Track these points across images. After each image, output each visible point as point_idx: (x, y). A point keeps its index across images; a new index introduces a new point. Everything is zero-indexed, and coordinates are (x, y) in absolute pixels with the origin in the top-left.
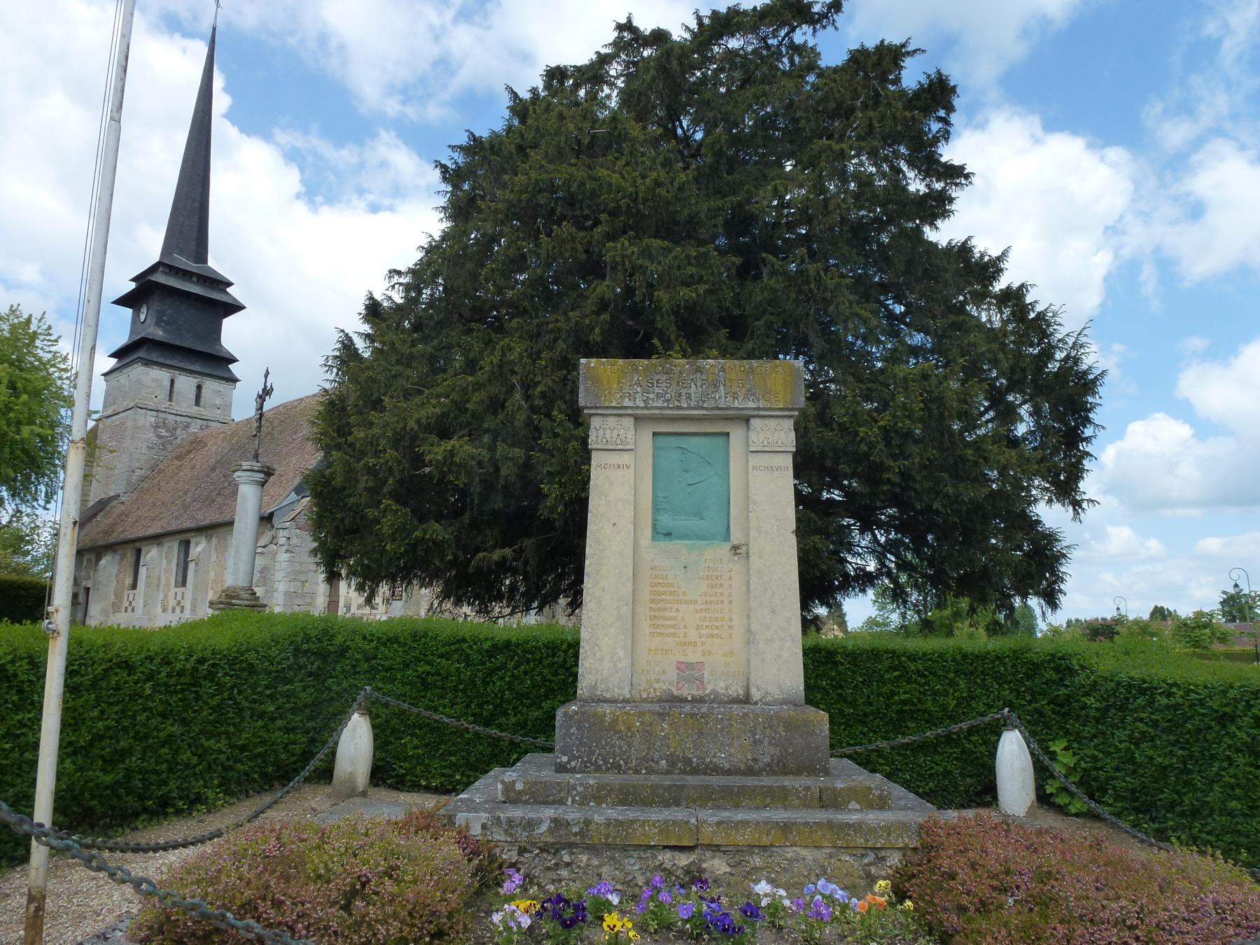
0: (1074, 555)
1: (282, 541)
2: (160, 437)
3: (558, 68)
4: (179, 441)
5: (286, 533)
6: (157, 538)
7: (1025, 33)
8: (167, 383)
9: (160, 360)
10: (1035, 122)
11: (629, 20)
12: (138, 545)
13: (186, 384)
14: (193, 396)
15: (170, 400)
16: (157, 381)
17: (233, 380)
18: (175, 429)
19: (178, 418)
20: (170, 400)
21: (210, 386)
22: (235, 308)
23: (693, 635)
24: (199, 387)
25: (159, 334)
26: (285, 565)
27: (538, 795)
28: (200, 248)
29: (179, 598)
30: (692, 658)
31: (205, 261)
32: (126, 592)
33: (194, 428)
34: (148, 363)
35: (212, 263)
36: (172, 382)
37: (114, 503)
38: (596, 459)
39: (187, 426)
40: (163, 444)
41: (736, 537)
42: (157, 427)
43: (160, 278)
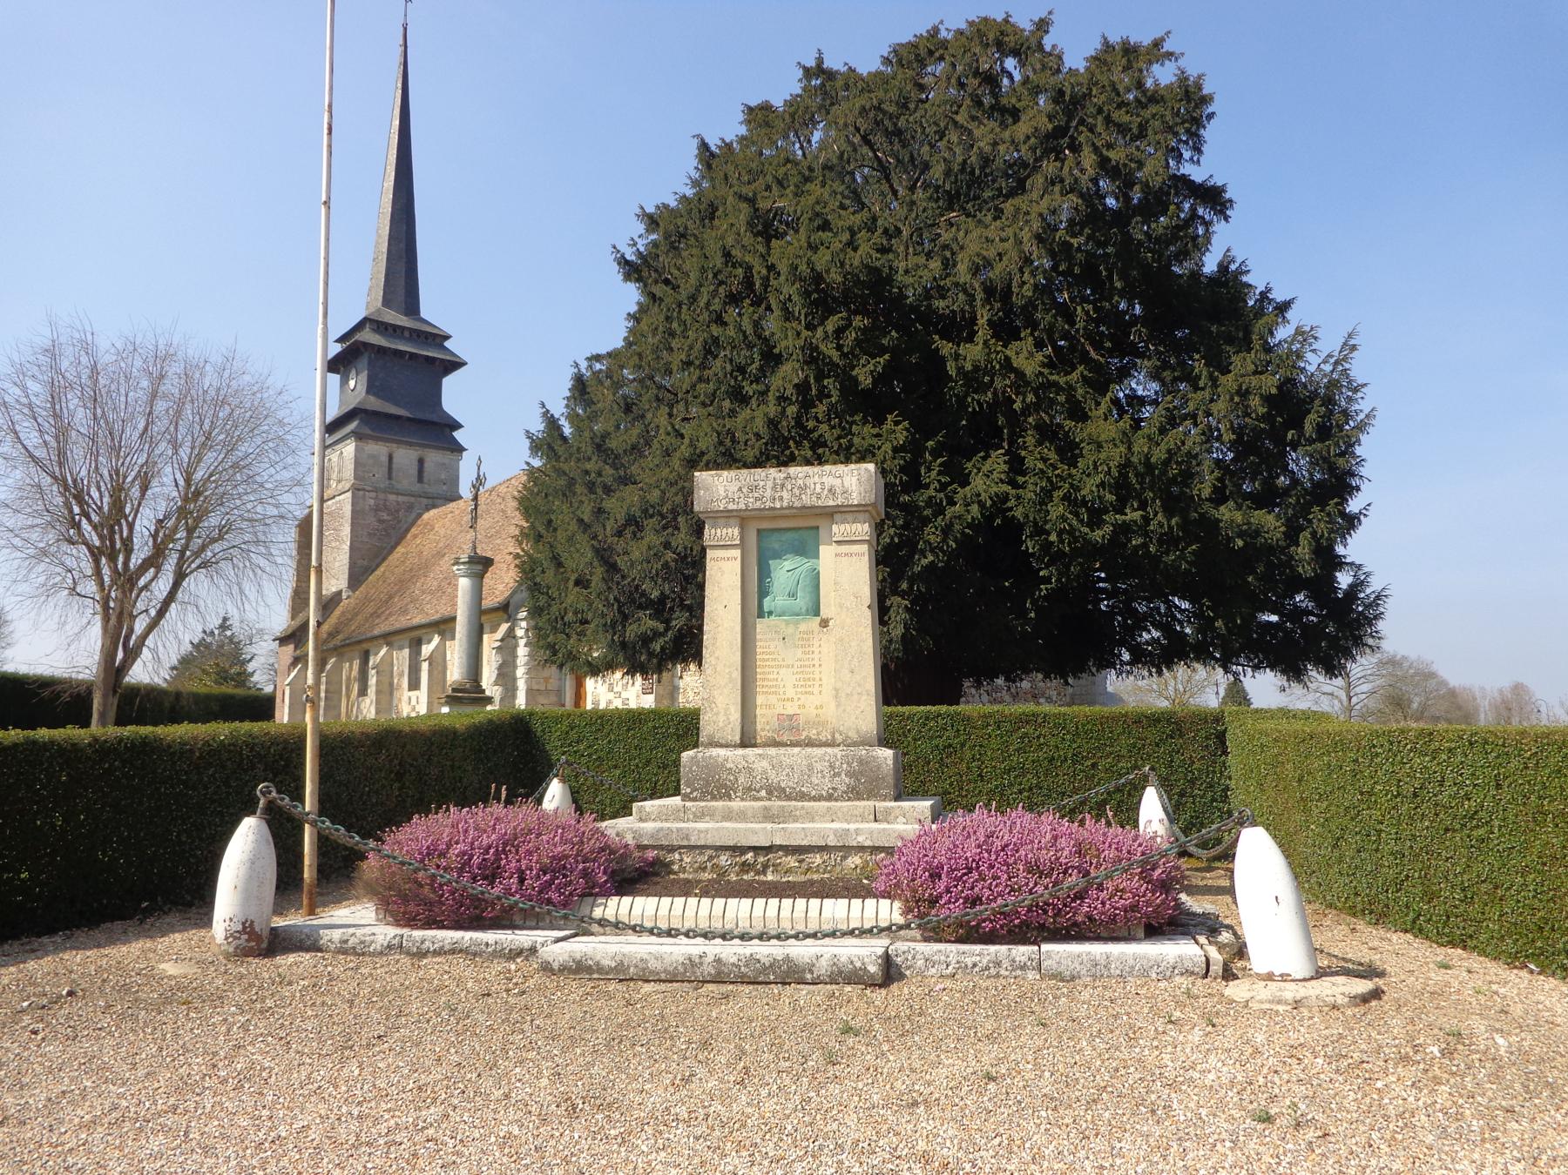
0: (1390, 608)
2: (380, 521)
6: (388, 638)
8: (384, 459)
11: (820, 61)
12: (365, 646)
14: (414, 471)
15: (390, 478)
17: (459, 449)
19: (400, 499)
20: (390, 478)
21: (434, 458)
22: (455, 365)
23: (790, 693)
24: (421, 462)
25: (375, 404)
27: (678, 815)
28: (411, 304)
29: (414, 702)
30: (790, 711)
35: (426, 312)
36: (390, 458)
38: (710, 554)
41: (824, 613)
42: (376, 509)
43: (368, 336)
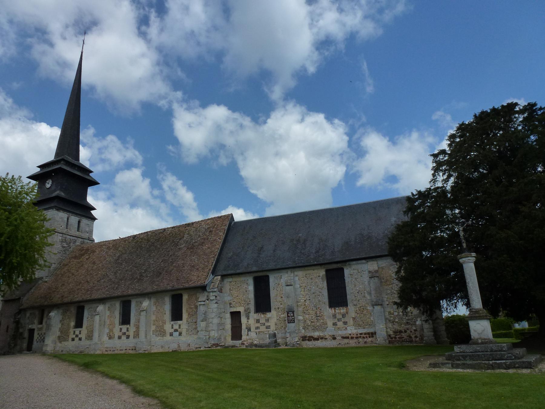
1: (212, 298)
2: (63, 247)
3: (482, 113)
4: (71, 249)
5: (214, 294)
6: (102, 301)
7: (293, 76)
9: (63, 208)
10: (304, 109)
13: (74, 220)
16: (62, 218)
17: (94, 219)
18: (70, 243)
19: (71, 238)
21: (84, 221)
24: (79, 222)
26: (215, 310)
31: (79, 161)
32: (72, 331)
33: (78, 243)
34: (58, 209)
37: (40, 282)
39: (75, 242)
40: (64, 251)
